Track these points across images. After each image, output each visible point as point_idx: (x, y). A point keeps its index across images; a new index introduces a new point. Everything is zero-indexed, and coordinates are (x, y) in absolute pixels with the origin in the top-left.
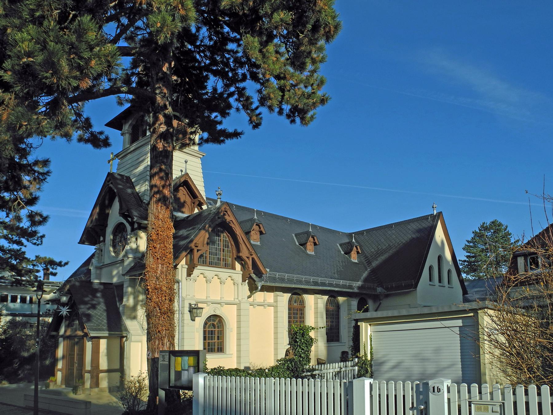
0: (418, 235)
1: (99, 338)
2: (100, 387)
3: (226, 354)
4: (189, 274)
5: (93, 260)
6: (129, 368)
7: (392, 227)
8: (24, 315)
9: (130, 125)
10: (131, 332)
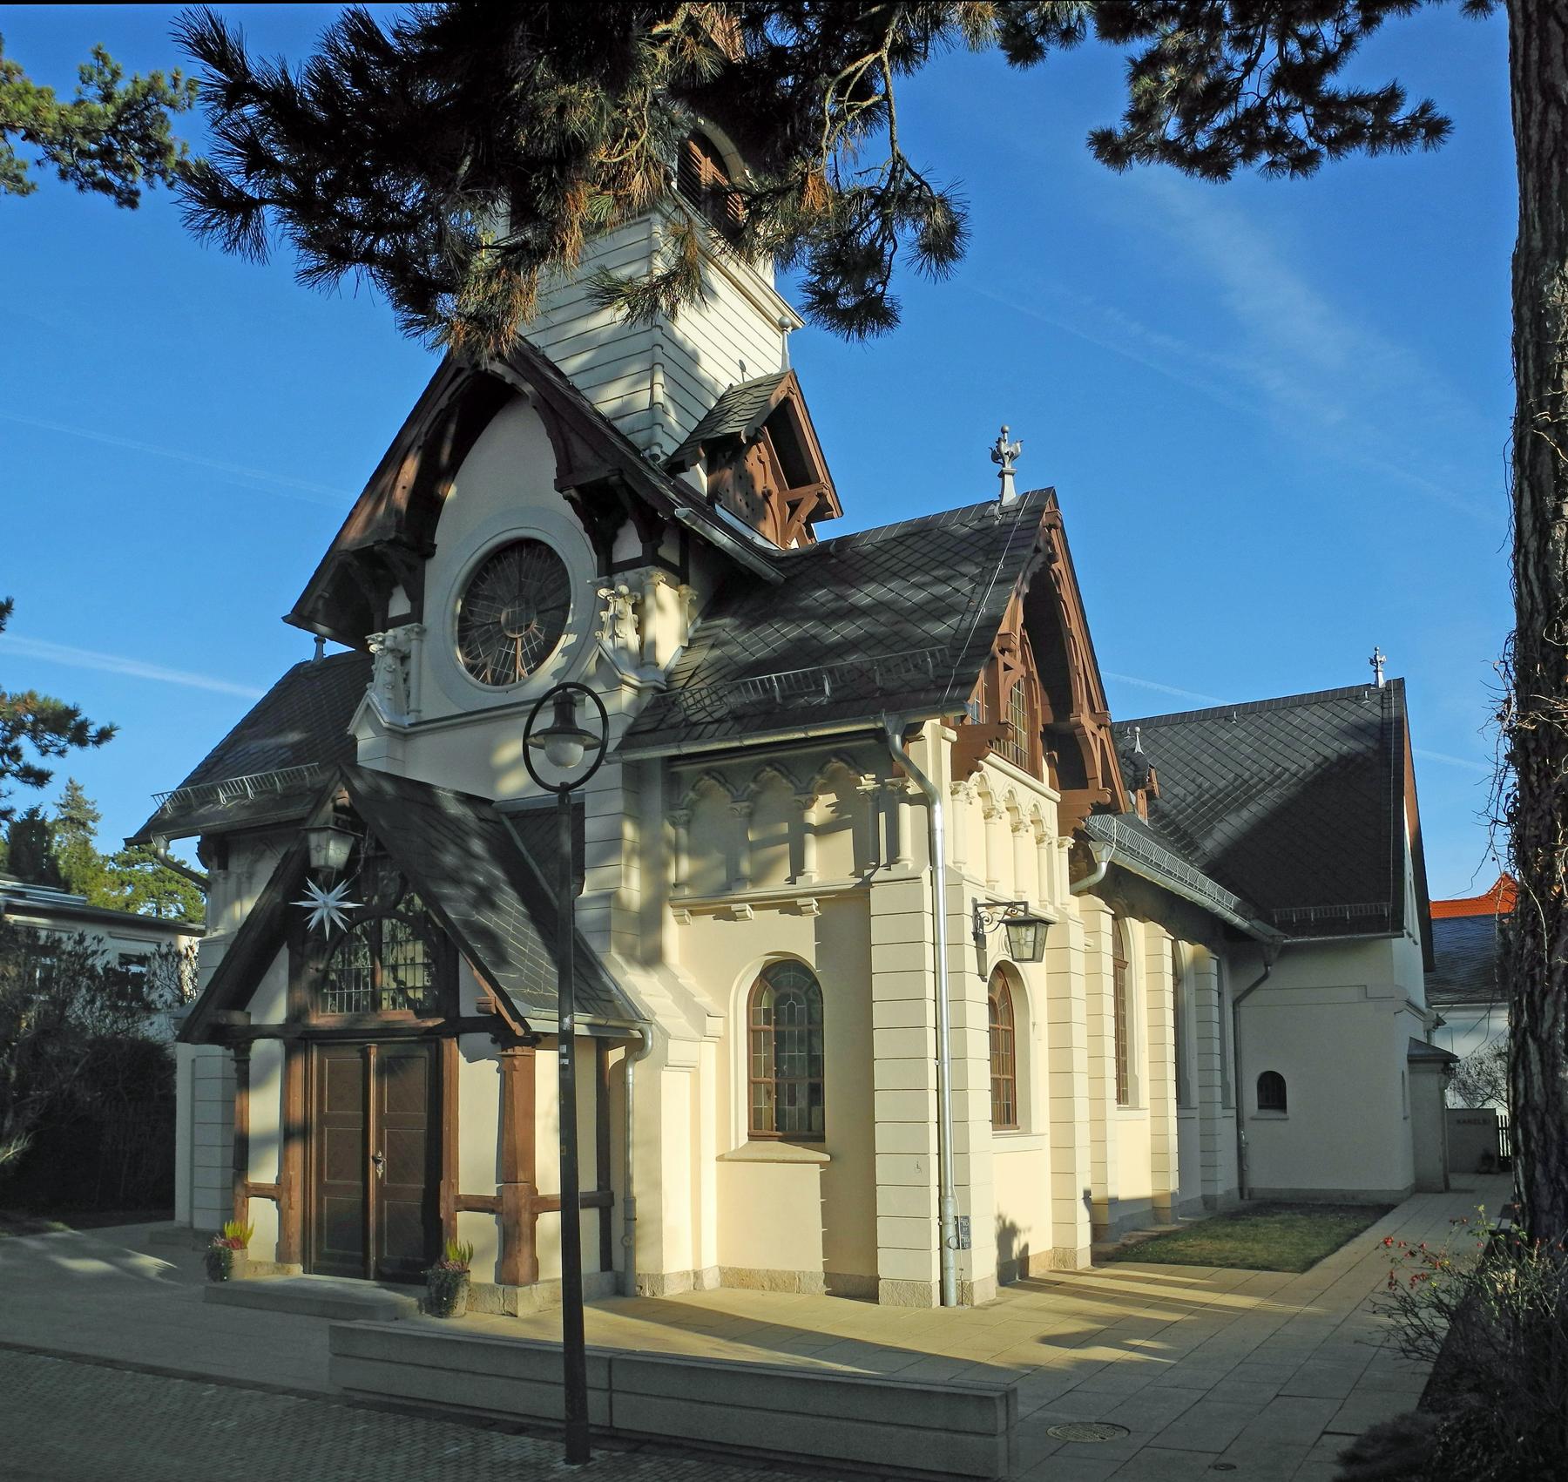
0: (1348, 746)
4: (965, 765)
6: (657, 1185)
7: (1228, 718)
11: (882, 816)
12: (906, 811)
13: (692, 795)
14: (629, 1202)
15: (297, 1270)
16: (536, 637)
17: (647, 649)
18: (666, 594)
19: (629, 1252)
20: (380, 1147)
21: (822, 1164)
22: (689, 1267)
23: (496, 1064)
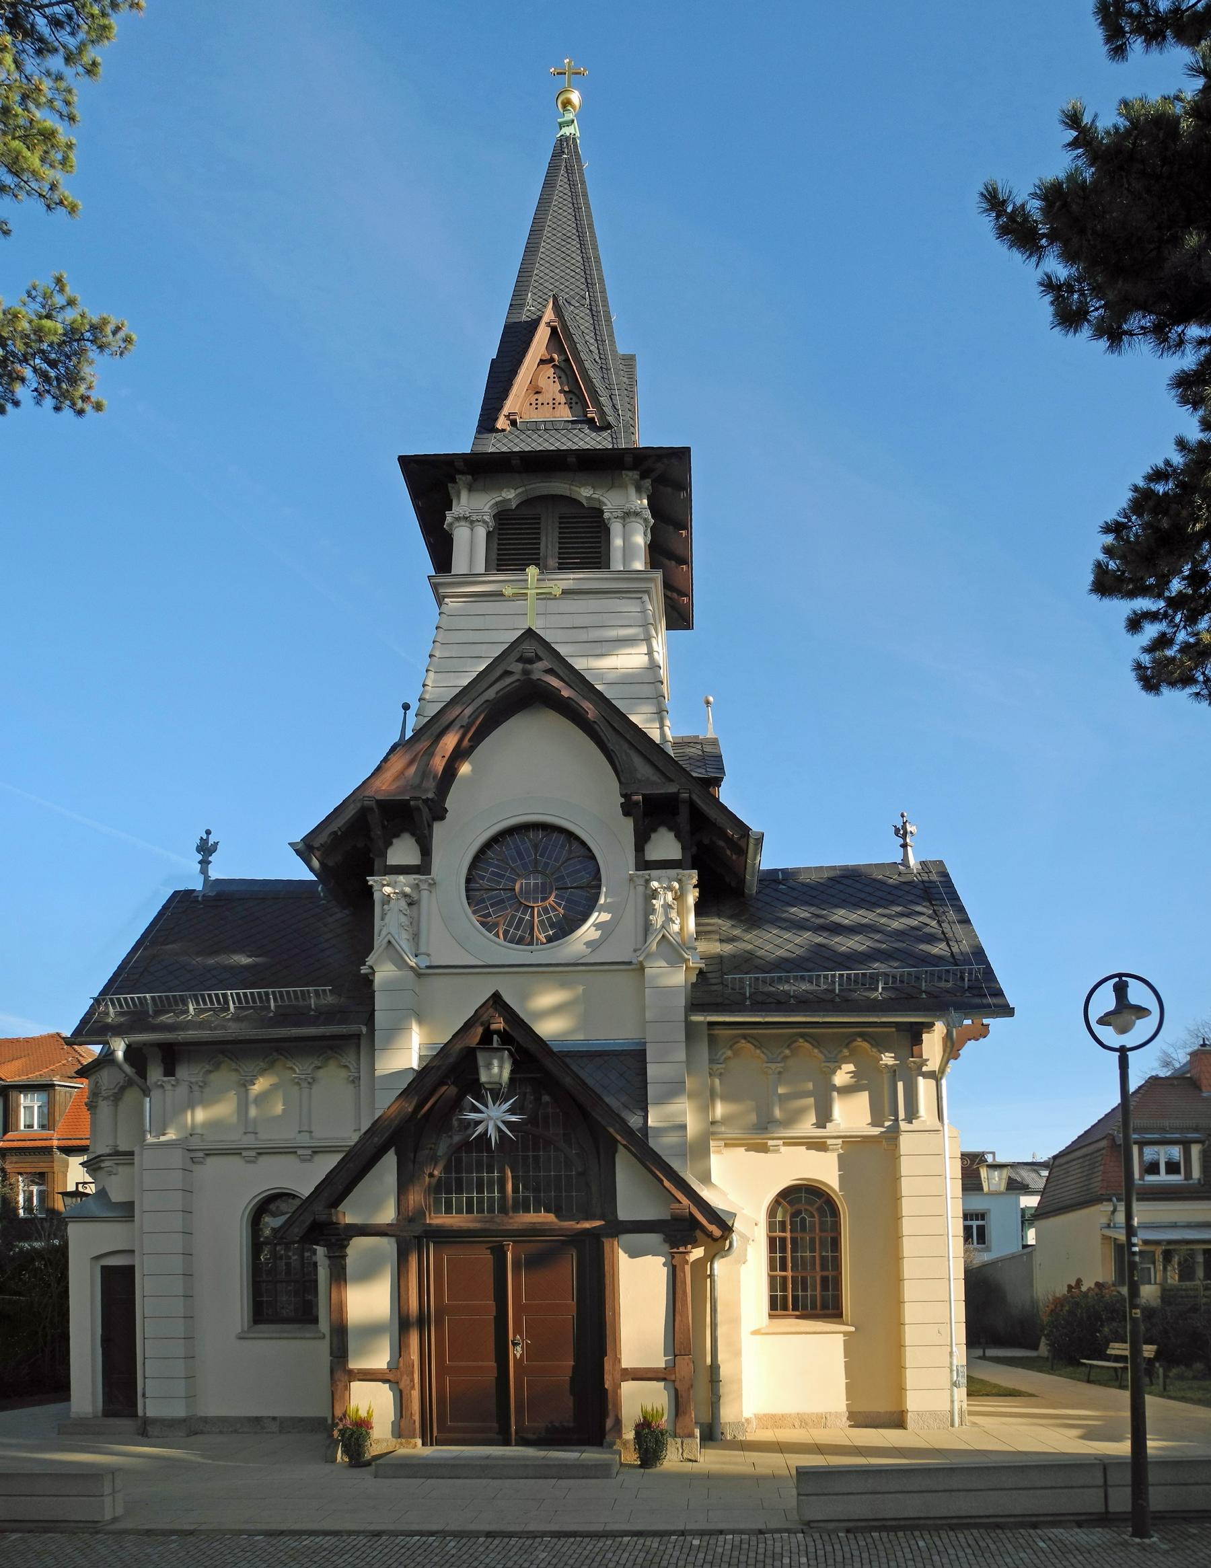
6: (738, 1354)
11: (900, 1085)
16: (554, 909)
21: (845, 1334)
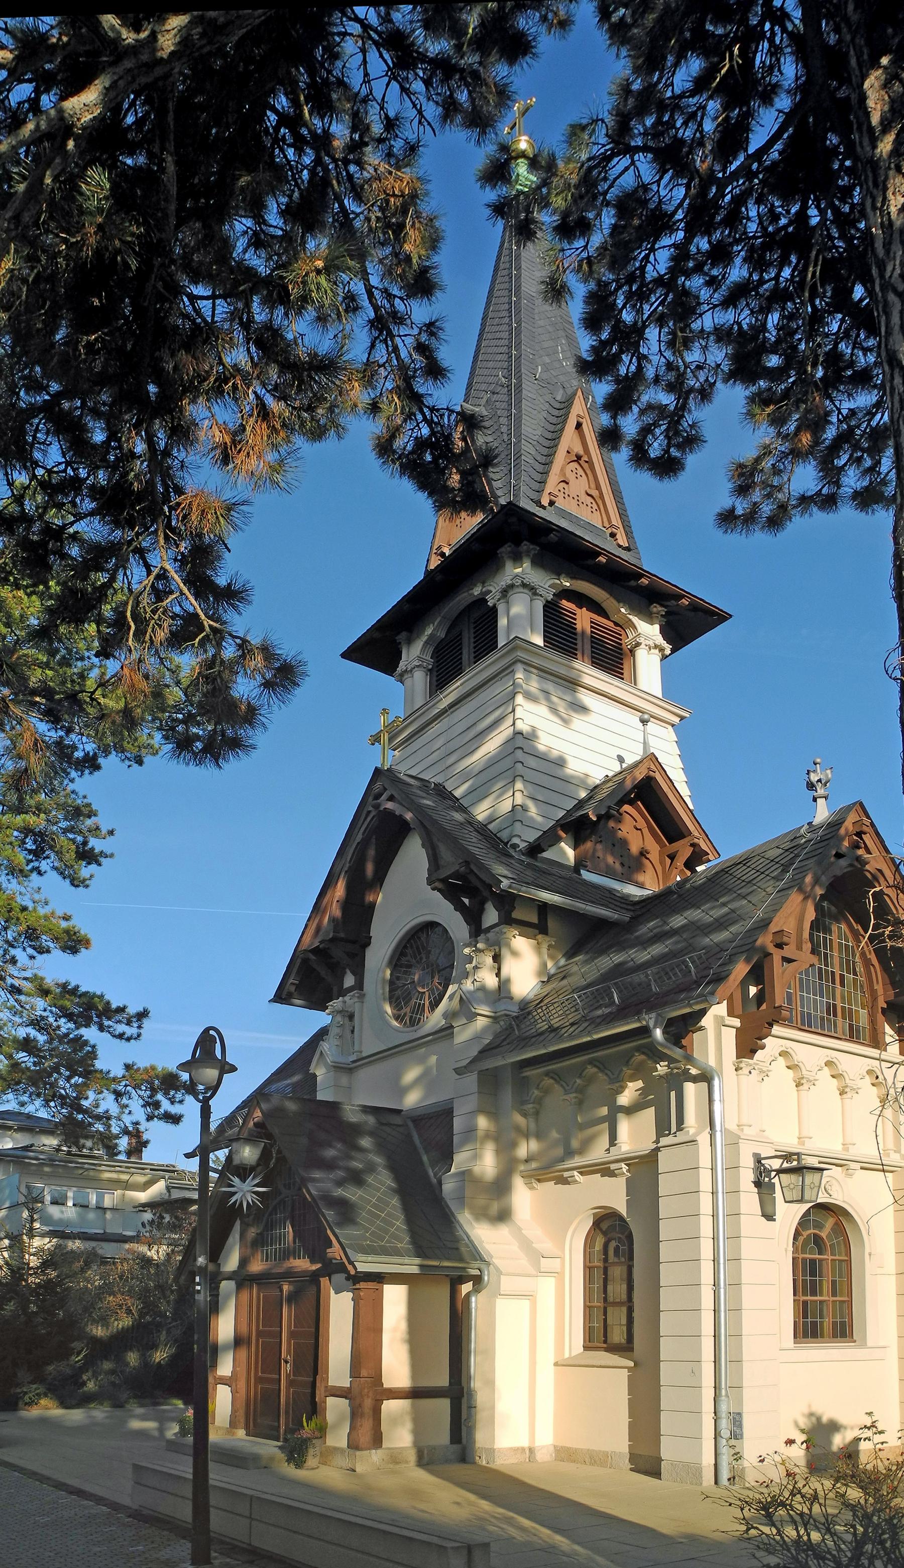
1: (379, 1278)
2: (385, 1444)
3: (864, 1345)
4: (748, 1047)
5: (325, 1046)
6: (490, 1383)
8: (84, 1237)
9: (426, 643)
10: (495, 1261)
11: (673, 1094)
12: (690, 1088)
13: (536, 1092)
14: (471, 1394)
15: (241, 1433)
17: (504, 985)
18: (521, 943)
19: (471, 1430)
20: (289, 1352)
22: (525, 1444)
23: (351, 1295)
